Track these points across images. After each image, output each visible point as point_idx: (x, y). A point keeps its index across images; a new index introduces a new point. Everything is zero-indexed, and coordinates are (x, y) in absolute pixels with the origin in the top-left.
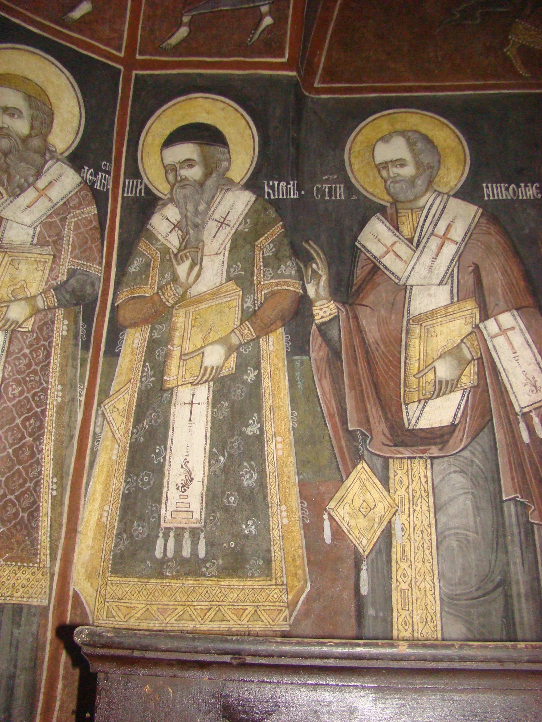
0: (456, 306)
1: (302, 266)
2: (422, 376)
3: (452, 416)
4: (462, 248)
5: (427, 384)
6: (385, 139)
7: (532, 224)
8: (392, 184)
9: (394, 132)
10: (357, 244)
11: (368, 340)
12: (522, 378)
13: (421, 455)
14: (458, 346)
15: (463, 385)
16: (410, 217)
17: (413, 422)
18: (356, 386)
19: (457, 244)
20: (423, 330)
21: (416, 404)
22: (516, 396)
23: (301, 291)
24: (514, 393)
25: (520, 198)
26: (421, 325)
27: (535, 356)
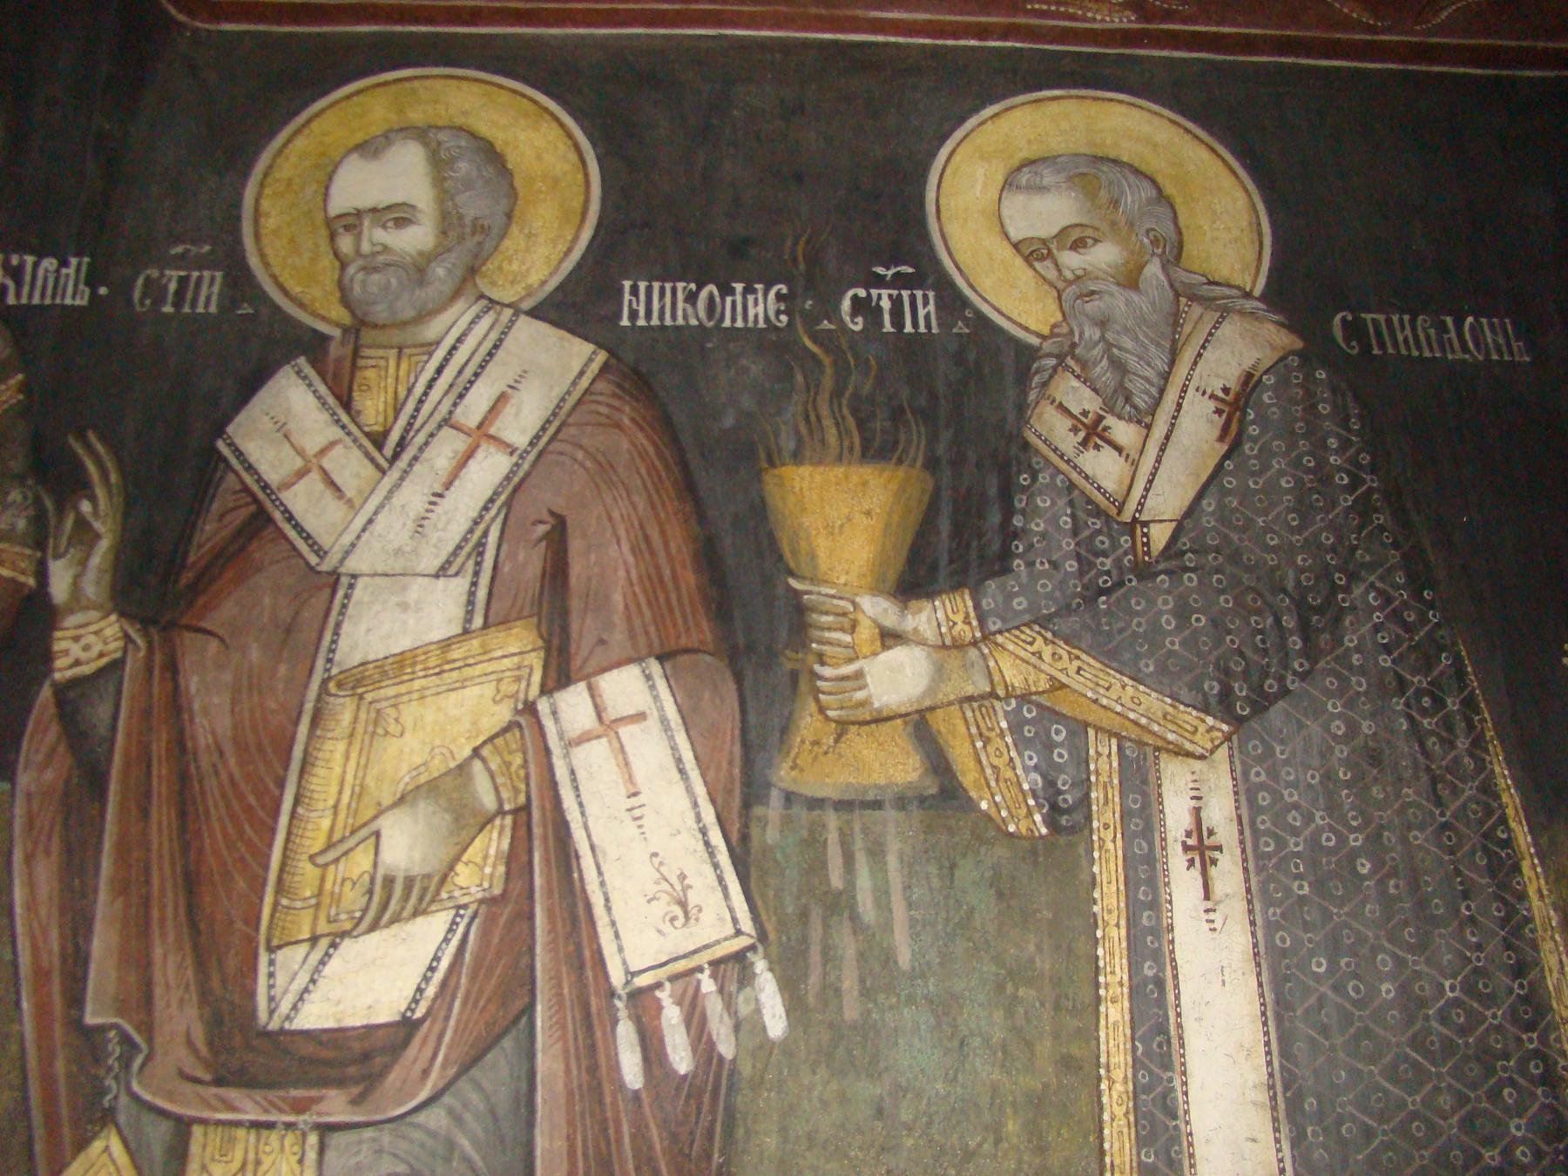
0: (475, 643)
1: (49, 504)
2: (337, 860)
3: (409, 992)
4: (526, 466)
5: (348, 885)
6: (369, 148)
7: (747, 402)
8: (360, 276)
9: (401, 130)
10: (220, 445)
11: (193, 738)
12: (645, 874)
13: (291, 1118)
14: (460, 767)
15: (457, 893)
16: (392, 370)
17: (285, 1007)
18: (133, 884)
19: (511, 454)
20: (363, 715)
21: (302, 949)
22: (617, 936)
23: (31, 582)
24: (613, 923)
25: (727, 323)
26: (361, 697)
27: (695, 805)
